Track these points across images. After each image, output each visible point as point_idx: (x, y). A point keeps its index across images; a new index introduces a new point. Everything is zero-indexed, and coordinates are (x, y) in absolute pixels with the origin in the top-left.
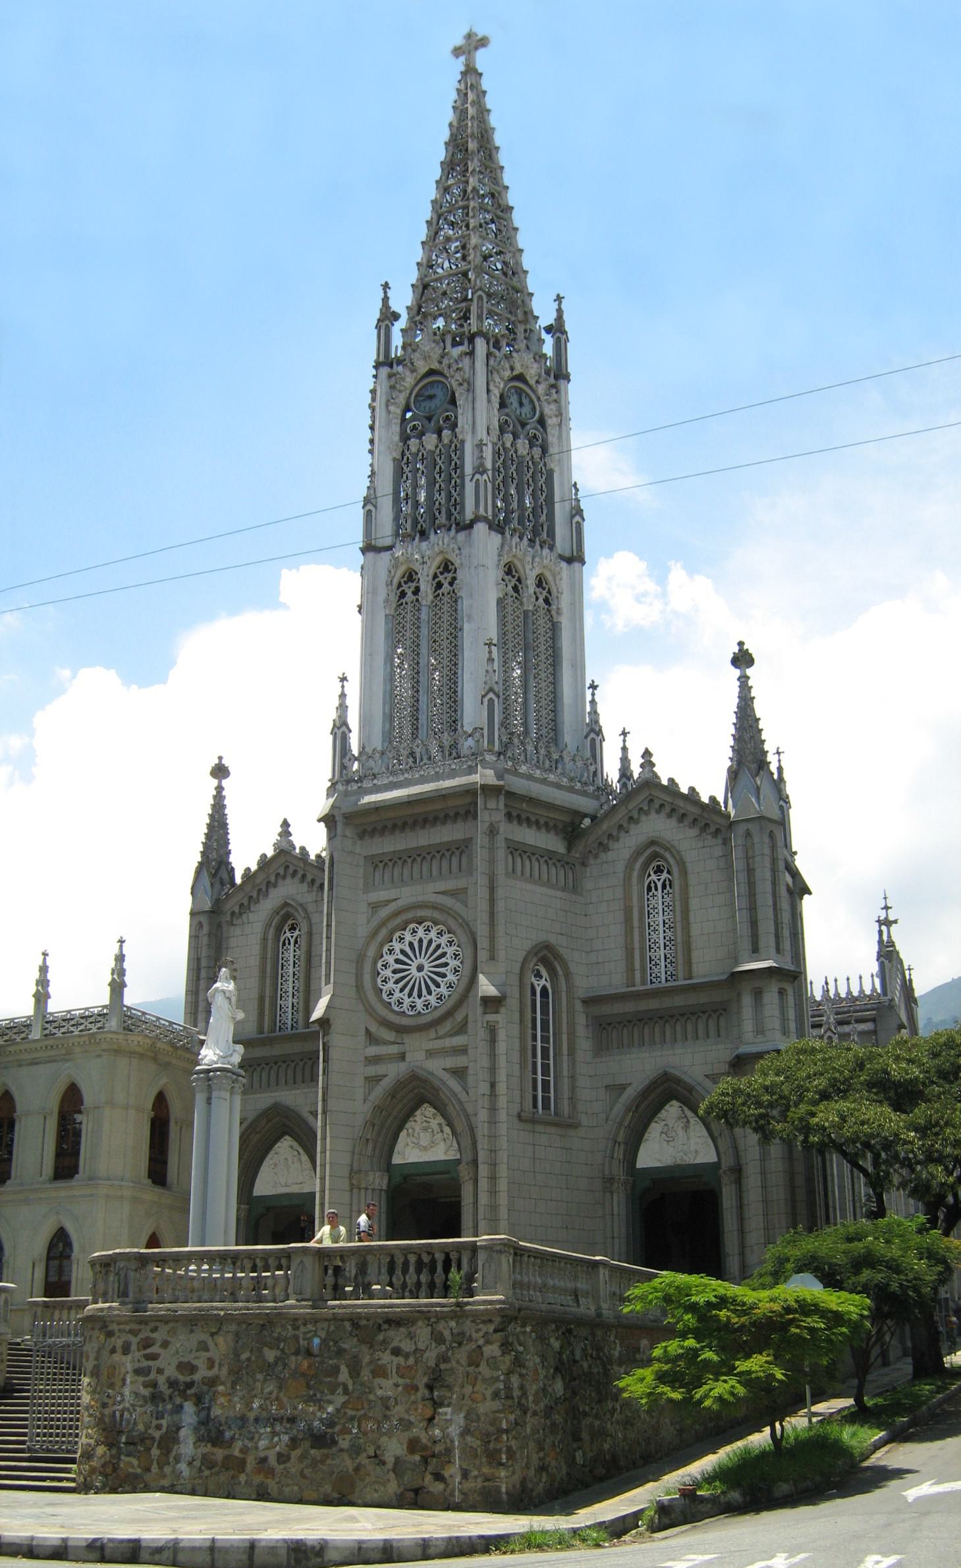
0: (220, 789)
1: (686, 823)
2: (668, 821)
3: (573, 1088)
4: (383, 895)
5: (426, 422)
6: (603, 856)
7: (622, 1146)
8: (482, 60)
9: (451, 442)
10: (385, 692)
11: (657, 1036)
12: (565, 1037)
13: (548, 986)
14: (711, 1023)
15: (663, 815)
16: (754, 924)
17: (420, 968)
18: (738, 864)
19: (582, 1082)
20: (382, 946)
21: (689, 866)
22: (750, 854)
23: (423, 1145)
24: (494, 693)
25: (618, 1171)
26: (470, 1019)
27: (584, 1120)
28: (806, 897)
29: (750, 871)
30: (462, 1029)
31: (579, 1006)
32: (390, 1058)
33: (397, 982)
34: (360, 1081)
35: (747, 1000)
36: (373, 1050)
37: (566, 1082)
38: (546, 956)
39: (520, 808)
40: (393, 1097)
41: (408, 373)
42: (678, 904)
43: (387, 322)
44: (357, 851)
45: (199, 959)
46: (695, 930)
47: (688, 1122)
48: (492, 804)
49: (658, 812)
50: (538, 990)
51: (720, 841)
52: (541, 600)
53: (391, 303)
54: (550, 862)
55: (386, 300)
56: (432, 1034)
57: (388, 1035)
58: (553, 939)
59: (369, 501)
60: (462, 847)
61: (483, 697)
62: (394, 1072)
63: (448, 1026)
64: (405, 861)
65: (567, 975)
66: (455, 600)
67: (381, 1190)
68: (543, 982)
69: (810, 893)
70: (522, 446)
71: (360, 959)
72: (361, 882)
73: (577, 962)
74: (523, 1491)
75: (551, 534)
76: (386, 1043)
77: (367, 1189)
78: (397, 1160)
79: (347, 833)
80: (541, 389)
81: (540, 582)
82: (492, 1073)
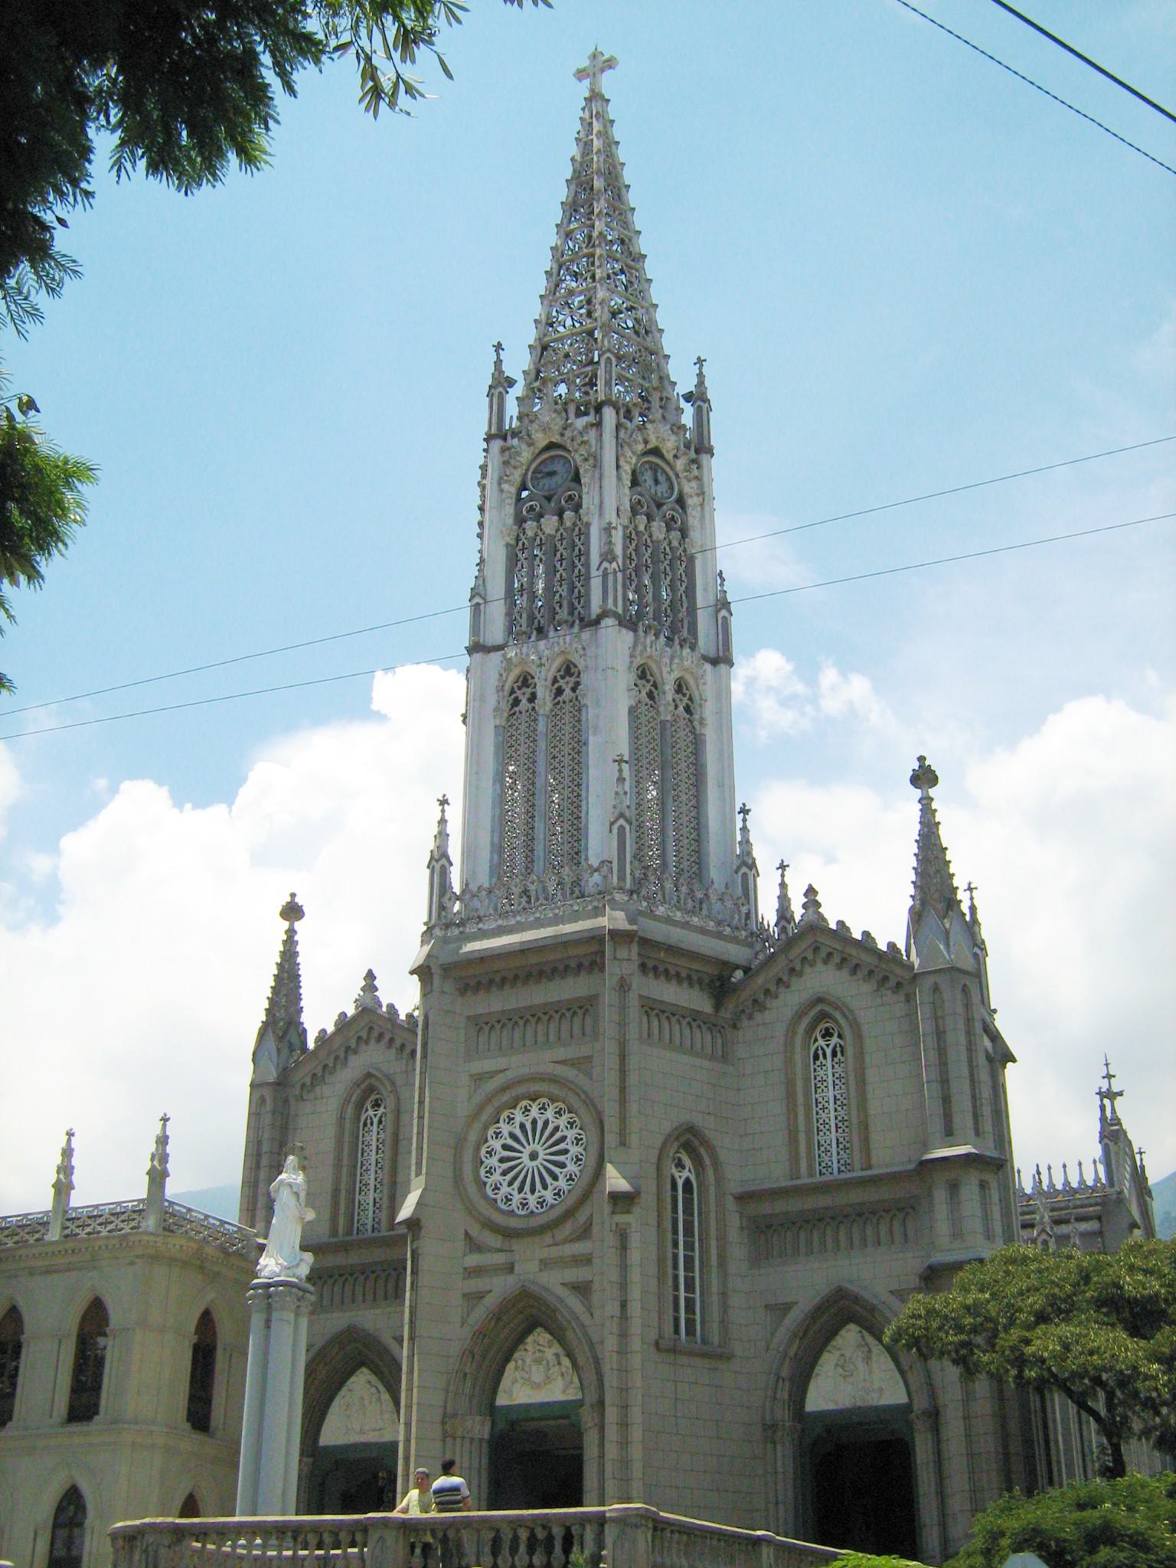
0: (291, 933)
3: (725, 1308)
4: (489, 1065)
7: (787, 1384)
9: (575, 525)
13: (693, 1178)
15: (831, 966)
16: (946, 1100)
19: (735, 1301)
21: (865, 1029)
23: (535, 1382)
24: (627, 820)
25: (783, 1414)
27: (738, 1350)
28: (1009, 1065)
30: (585, 1233)
31: (731, 1204)
32: (496, 1270)
35: (940, 1195)
36: (473, 1260)
38: (690, 1141)
39: (657, 958)
40: (499, 1319)
47: (870, 1351)
48: (622, 953)
49: (825, 962)
50: (680, 1183)
52: (681, 708)
54: (694, 1024)
55: (498, 363)
56: (548, 1238)
57: (494, 1240)
58: (698, 1121)
59: (478, 593)
60: (586, 1006)
62: (500, 1287)
63: (567, 1229)
65: (716, 1163)
66: (579, 708)
68: (685, 1174)
70: (658, 529)
76: (491, 1250)
78: (501, 1400)
80: (680, 464)
81: (680, 687)
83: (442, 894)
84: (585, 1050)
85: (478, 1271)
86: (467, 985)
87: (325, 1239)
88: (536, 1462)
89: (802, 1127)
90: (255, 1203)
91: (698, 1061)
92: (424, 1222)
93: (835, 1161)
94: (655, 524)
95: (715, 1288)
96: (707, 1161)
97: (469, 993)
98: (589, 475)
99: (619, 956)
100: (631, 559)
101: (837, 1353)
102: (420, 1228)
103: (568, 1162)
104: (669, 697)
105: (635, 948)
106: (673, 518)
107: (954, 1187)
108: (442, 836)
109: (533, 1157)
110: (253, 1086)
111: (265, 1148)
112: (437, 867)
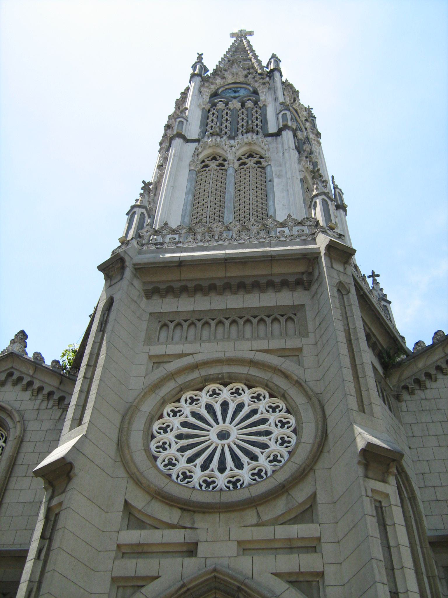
6: (419, 394)
17: (223, 435)
20: (164, 403)
26: (321, 498)
30: (307, 512)
32: (166, 551)
33: (184, 424)
36: (133, 536)
56: (251, 516)
60: (290, 315)
61: (278, 114)
63: (280, 507)
71: (128, 415)
72: (143, 334)
74: (389, 465)
84: (292, 343)
85: (139, 551)
92: (78, 465)
109: (225, 435)
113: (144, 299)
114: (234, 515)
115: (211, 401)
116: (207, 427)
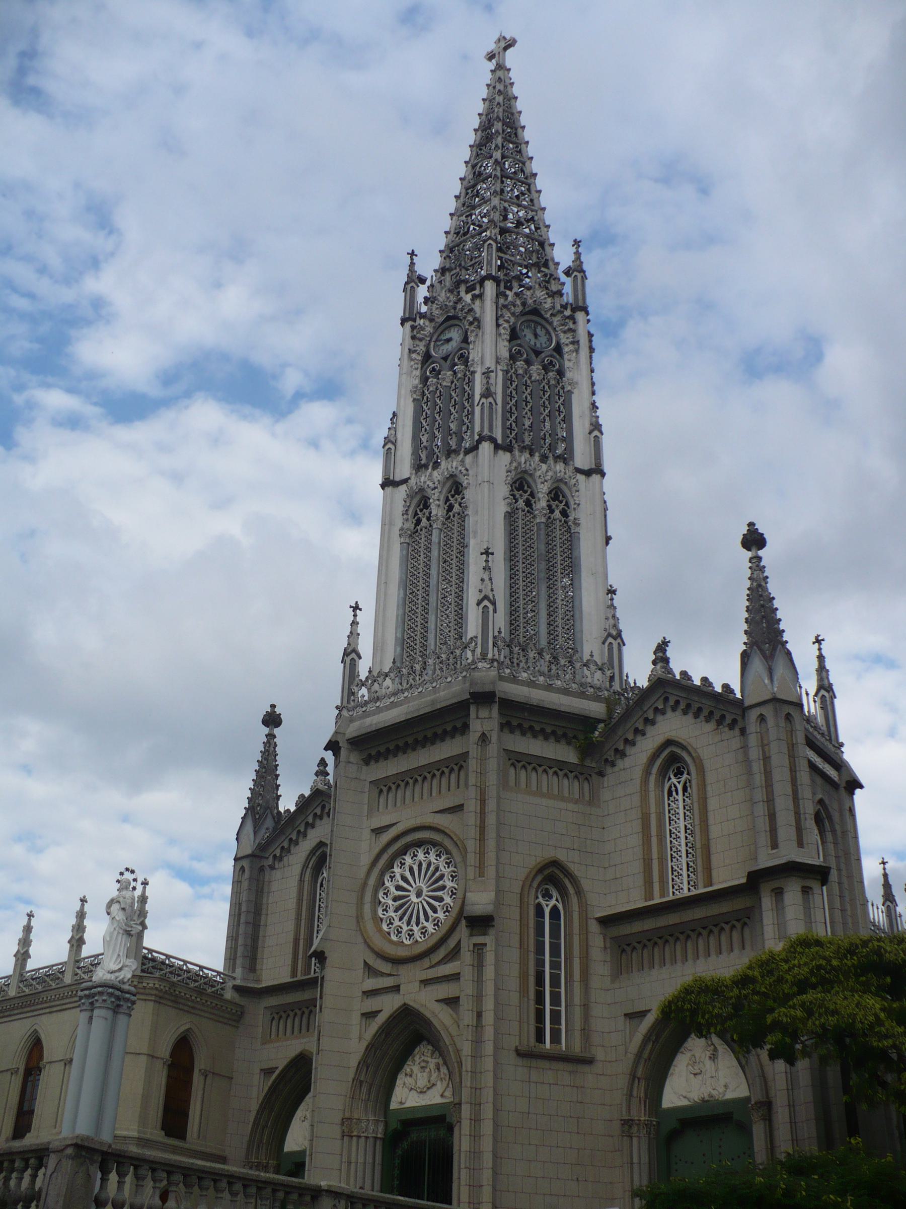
0: (271, 736)
1: (702, 718)
2: (684, 718)
3: (586, 1017)
4: (385, 821)
5: (442, 362)
6: (620, 764)
7: (643, 1083)
8: (511, 58)
9: (465, 375)
10: (397, 616)
11: (678, 953)
12: (576, 962)
13: (560, 906)
14: (735, 935)
15: (679, 712)
16: (772, 817)
17: (419, 894)
18: (755, 753)
19: (597, 1011)
21: (707, 764)
22: (765, 742)
23: (417, 1089)
24: (489, 600)
25: (640, 1114)
27: (599, 1054)
28: (858, 791)
29: (766, 759)
31: (594, 927)
34: (356, 1018)
35: (767, 902)
37: (578, 1012)
38: (553, 876)
39: (520, 716)
41: (427, 323)
42: (696, 806)
43: (413, 284)
44: (363, 777)
45: (240, 904)
46: (715, 831)
47: (715, 1049)
48: (484, 713)
49: (674, 709)
50: (547, 911)
51: (737, 731)
52: (557, 512)
53: (416, 268)
54: (560, 773)
55: (412, 264)
56: (426, 962)
57: (385, 967)
58: (562, 856)
59: (390, 442)
60: (459, 763)
62: (389, 1005)
63: (442, 953)
64: (407, 783)
65: (579, 892)
66: (463, 517)
67: (376, 1138)
68: (553, 902)
69: (861, 787)
70: (536, 370)
73: (588, 877)
75: (570, 450)
76: (383, 974)
77: (359, 1137)
79: (352, 759)
80: (556, 321)
81: (556, 494)
82: (483, 1004)
83: (351, 683)
86: (370, 755)
87: (288, 980)
88: (419, 1156)
89: (655, 855)
90: (236, 952)
91: (563, 805)
93: (686, 883)
94: (533, 368)
95: (577, 1000)
96: (571, 890)
97: (372, 763)
98: (474, 334)
99: (480, 715)
100: (511, 397)
101: (689, 1054)
102: (325, 958)
103: (444, 897)
104: (543, 503)
105: (495, 709)
106: (551, 363)
107: (779, 893)
108: (353, 635)
110: (236, 859)
111: (244, 908)
112: (348, 660)
113: (364, 768)
114: (418, 963)
115: (391, 896)
116: (410, 888)
